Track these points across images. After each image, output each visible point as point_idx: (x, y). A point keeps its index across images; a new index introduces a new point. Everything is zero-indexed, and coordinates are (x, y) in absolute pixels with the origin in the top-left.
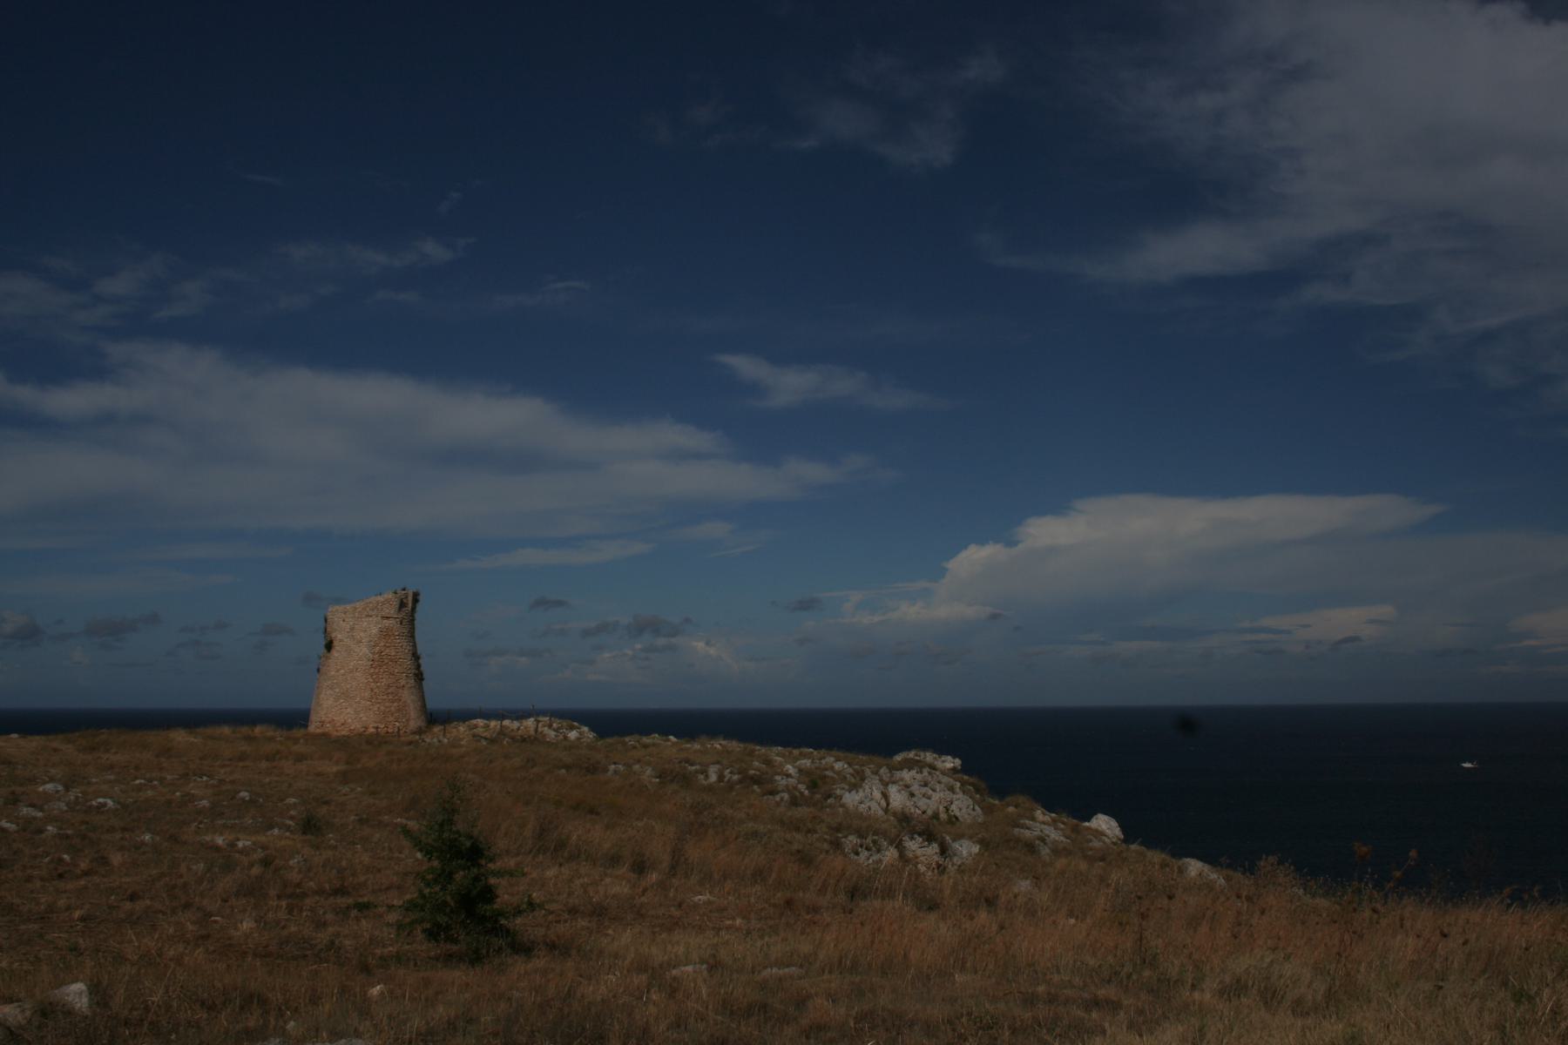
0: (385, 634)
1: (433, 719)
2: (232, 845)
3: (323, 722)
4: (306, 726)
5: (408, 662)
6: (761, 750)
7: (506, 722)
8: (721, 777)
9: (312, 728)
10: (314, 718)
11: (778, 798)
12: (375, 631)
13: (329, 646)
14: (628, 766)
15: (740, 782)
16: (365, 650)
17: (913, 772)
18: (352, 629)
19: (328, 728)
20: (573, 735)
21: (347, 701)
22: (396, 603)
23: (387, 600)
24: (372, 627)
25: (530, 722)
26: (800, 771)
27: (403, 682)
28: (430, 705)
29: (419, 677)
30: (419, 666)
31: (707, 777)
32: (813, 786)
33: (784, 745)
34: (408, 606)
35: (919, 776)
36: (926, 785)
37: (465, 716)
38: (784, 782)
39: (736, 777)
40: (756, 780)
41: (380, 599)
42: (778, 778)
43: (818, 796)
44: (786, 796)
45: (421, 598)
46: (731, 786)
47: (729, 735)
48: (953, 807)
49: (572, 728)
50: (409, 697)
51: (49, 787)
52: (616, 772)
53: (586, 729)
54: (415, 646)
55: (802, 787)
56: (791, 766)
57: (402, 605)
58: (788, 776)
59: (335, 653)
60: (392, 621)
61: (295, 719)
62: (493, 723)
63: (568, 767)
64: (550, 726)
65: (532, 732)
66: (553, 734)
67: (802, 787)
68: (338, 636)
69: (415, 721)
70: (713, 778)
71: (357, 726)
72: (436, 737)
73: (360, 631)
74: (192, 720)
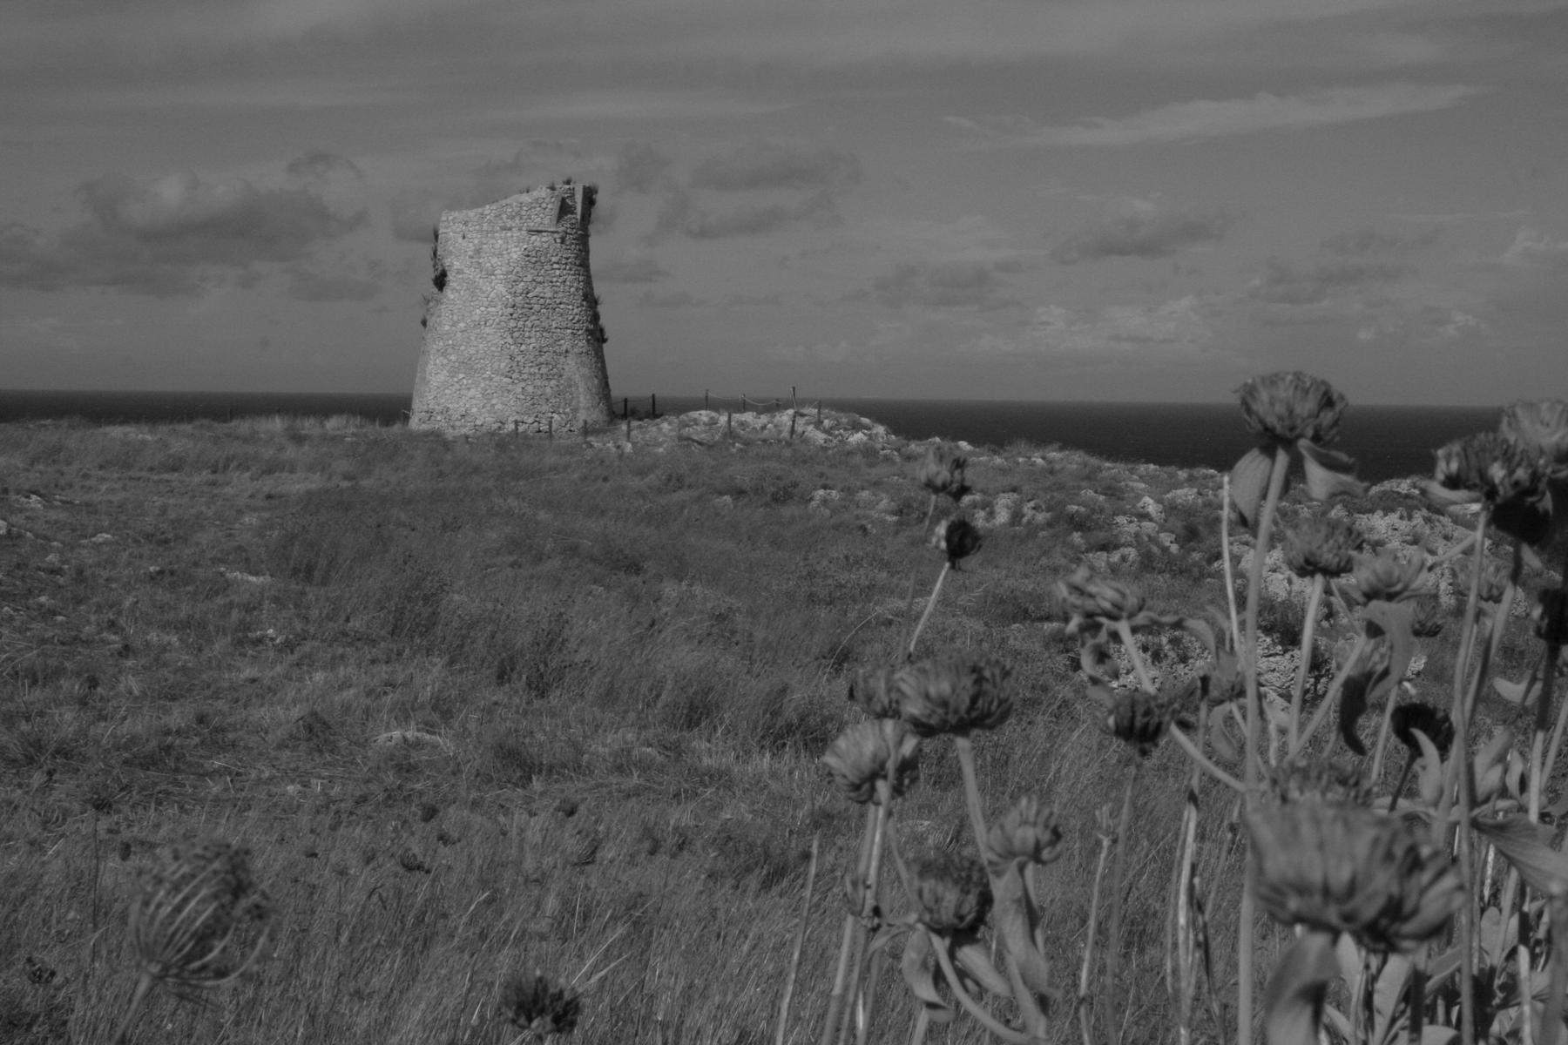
0: (534, 259)
1: (623, 412)
3: (430, 412)
4: (407, 418)
5: (575, 310)
6: (1111, 469)
7: (748, 417)
8: (1016, 516)
9: (415, 424)
10: (417, 405)
11: (1115, 557)
12: (516, 254)
13: (440, 281)
14: (849, 491)
15: (1049, 525)
16: (501, 289)
17: (1393, 518)
18: (478, 251)
19: (439, 423)
20: (858, 437)
21: (473, 374)
22: (553, 207)
23: (538, 204)
24: (510, 249)
25: (785, 417)
26: (1171, 509)
27: (566, 345)
28: (617, 392)
29: (597, 336)
31: (992, 514)
32: (1190, 535)
33: (1161, 460)
34: (579, 215)
35: (1404, 525)
36: (1415, 542)
37: (681, 407)
38: (1133, 528)
39: (1041, 517)
40: (1077, 523)
41: (526, 198)
42: (1121, 520)
43: (1196, 556)
44: (1132, 553)
45: (600, 198)
46: (1033, 530)
47: (1067, 443)
49: (857, 427)
50: (576, 370)
52: (825, 502)
53: (880, 429)
54: (588, 282)
55: (1166, 539)
56: (1150, 497)
57: (564, 209)
58: (1144, 516)
59: (449, 293)
60: (545, 238)
61: (393, 410)
62: (723, 419)
63: (739, 493)
64: (818, 424)
65: (785, 434)
66: (819, 437)
67: (1166, 539)
68: (454, 264)
69: (587, 410)
70: (1002, 517)
71: (486, 420)
72: (628, 439)
73: (493, 254)
74: (321, 407)
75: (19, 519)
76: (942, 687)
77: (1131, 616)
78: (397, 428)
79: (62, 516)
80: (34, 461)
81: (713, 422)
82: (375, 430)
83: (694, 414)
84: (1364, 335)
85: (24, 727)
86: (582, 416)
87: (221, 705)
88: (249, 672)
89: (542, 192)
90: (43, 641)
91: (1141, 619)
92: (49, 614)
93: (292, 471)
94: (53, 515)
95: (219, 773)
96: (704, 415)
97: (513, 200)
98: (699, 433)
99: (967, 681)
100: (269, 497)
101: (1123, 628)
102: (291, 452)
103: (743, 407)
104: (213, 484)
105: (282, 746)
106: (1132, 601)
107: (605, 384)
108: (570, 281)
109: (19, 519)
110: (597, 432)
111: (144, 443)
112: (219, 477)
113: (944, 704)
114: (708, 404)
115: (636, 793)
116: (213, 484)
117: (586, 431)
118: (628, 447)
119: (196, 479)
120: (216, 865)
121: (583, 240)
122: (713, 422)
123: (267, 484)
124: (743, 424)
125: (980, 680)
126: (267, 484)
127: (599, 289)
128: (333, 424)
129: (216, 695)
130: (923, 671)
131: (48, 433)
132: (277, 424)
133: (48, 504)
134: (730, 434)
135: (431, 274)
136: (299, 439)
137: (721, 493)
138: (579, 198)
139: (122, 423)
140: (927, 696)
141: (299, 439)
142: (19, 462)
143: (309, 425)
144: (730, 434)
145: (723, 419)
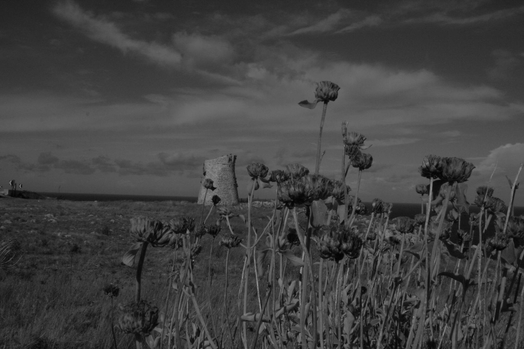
0: (224, 170)
2: (63, 236)
4: (197, 202)
5: (231, 180)
7: (266, 203)
9: (199, 203)
10: (199, 199)
16: (217, 176)
18: (212, 168)
22: (227, 159)
23: (225, 159)
24: (219, 168)
27: (230, 187)
28: (240, 197)
29: (236, 186)
30: (236, 182)
41: (222, 158)
45: (237, 158)
48: (412, 239)
50: (231, 192)
51: (48, 215)
54: (234, 175)
57: (230, 160)
61: (194, 200)
62: (261, 203)
68: (207, 170)
69: (233, 200)
71: (346, 209)
74: (180, 199)
75: (117, 220)
76: (178, 223)
77: (228, 214)
78: (195, 203)
79: (126, 219)
80: (121, 208)
81: (259, 204)
82: (190, 204)
83: (255, 202)
84: (394, 188)
85: (112, 260)
86: (232, 202)
87: (154, 257)
88: (160, 251)
89: (225, 156)
90: (119, 244)
91: (231, 215)
92: (121, 239)
93: (173, 211)
94: (124, 219)
95: (150, 271)
96: (257, 202)
97: (220, 158)
98: (256, 206)
99: (183, 222)
100: (168, 216)
101: (227, 217)
102: (173, 207)
103: (265, 201)
104: (157, 214)
105: (164, 266)
106: (228, 211)
107: (237, 195)
108: (231, 175)
109: (117, 220)
110: (235, 205)
111: (143, 205)
112: (158, 212)
113: (178, 226)
114: (260, 200)
115: (235, 277)
116: (157, 214)
117: (233, 205)
118: (242, 208)
119: (153, 213)
120: (11, 242)
121: (234, 166)
122: (259, 204)
123: (168, 214)
124: (265, 204)
125: (185, 221)
126: (168, 214)
127: (237, 176)
128: (182, 202)
129: (153, 256)
130: (174, 220)
131: (125, 203)
132: (171, 202)
133: (124, 217)
134: (263, 206)
135: (203, 173)
136: (175, 205)
137: (260, 218)
138: (233, 158)
139: (140, 201)
140: (175, 225)
141: (175, 205)
142: (118, 208)
143: (177, 203)
144: (263, 206)
145: (261, 203)
